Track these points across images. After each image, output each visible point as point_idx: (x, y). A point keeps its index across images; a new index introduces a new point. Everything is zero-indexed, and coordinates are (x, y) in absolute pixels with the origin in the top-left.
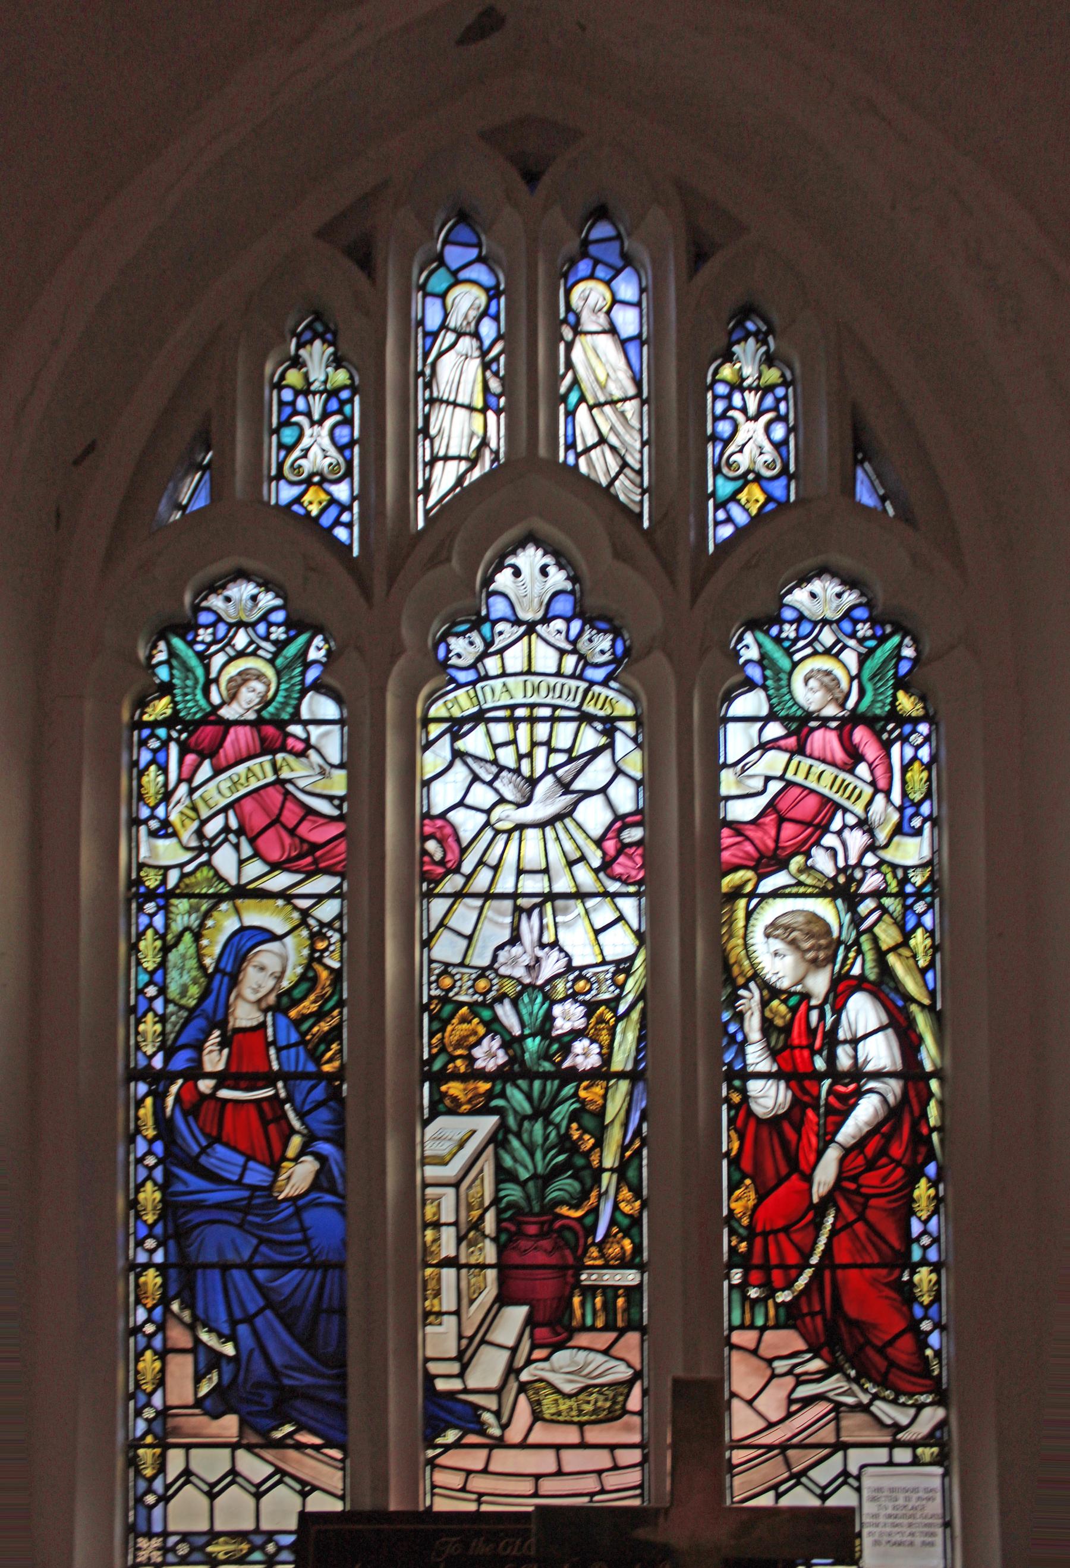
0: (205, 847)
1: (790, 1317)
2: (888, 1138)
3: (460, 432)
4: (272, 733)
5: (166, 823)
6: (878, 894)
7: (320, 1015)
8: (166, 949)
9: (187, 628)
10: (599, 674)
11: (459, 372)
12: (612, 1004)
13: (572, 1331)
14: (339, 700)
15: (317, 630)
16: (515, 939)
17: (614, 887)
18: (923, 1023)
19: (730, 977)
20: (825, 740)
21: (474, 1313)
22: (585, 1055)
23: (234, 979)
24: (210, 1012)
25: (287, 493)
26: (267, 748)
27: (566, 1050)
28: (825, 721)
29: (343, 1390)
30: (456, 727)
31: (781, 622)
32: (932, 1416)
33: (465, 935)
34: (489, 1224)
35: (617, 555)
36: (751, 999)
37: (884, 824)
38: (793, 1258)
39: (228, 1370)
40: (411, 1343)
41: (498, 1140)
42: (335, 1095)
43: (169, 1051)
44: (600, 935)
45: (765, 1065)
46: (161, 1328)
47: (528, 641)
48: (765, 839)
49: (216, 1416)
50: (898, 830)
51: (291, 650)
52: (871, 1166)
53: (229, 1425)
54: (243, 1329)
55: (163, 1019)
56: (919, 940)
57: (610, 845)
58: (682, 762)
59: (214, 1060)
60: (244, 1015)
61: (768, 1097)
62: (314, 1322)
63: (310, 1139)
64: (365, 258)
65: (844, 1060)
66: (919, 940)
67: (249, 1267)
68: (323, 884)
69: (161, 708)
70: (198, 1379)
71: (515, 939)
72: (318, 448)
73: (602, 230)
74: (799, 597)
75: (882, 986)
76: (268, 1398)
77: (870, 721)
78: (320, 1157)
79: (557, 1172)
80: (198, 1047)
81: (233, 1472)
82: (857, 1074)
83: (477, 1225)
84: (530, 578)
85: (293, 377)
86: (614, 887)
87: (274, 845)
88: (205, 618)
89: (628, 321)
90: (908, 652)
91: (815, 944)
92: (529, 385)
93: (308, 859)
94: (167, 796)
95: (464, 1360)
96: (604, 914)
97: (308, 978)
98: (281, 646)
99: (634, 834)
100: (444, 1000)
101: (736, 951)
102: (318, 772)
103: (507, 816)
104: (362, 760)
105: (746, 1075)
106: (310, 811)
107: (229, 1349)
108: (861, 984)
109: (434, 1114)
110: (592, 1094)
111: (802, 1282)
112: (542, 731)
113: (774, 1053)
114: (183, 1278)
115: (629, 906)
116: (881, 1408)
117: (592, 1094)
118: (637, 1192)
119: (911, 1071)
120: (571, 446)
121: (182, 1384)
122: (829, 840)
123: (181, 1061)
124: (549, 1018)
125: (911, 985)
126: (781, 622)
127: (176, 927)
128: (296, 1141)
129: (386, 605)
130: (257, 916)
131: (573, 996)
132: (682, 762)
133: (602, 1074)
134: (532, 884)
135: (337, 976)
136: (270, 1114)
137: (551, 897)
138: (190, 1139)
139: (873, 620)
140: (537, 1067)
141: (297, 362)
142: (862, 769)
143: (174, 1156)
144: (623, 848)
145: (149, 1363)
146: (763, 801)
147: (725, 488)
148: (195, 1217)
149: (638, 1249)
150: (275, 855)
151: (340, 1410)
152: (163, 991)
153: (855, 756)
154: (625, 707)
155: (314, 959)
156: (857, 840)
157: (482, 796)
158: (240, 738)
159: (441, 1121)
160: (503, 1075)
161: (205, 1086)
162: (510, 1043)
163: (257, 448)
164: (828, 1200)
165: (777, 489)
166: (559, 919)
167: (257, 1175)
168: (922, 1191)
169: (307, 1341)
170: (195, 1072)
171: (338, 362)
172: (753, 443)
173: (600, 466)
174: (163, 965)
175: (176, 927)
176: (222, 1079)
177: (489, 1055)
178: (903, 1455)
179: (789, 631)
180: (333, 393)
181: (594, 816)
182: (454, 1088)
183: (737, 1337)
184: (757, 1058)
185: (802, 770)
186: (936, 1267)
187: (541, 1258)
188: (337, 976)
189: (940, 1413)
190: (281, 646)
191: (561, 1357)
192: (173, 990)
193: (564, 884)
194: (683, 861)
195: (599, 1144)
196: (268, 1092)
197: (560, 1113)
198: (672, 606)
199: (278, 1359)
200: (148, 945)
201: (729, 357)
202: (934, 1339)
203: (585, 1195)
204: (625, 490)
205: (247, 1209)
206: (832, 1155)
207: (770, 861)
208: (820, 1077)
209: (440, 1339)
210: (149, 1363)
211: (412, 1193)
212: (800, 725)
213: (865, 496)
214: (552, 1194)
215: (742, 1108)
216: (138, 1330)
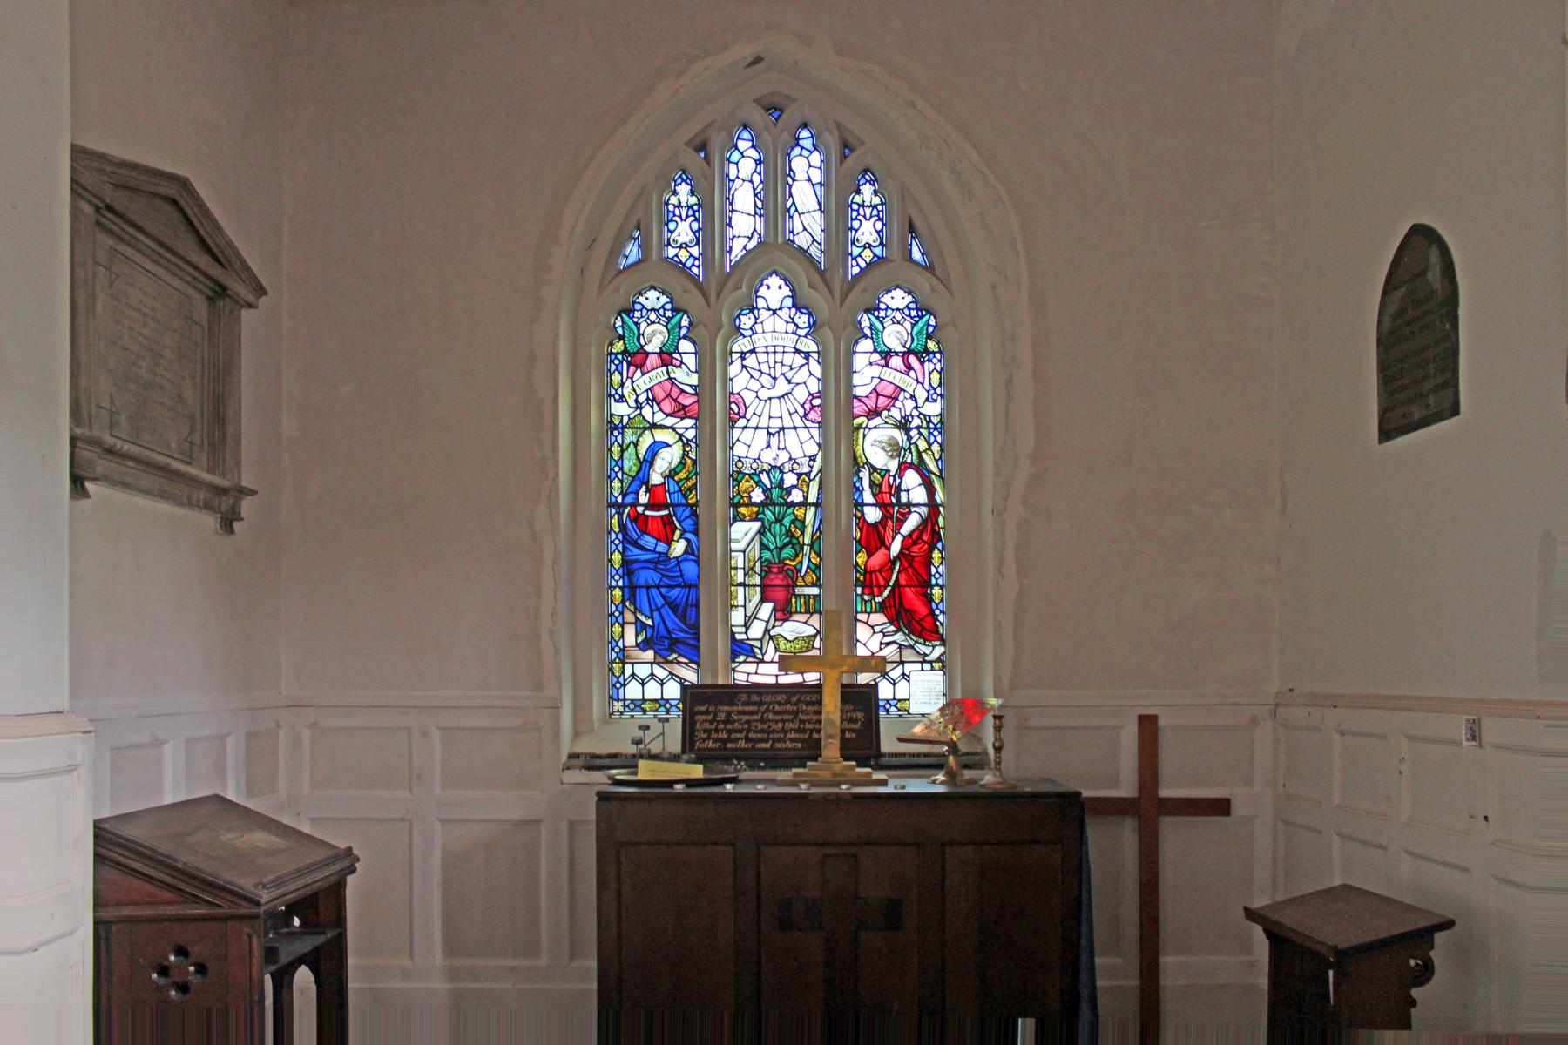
0: (639, 406)
1: (882, 608)
2: (921, 532)
3: (744, 226)
4: (667, 357)
5: (622, 396)
6: (918, 428)
7: (687, 479)
8: (623, 451)
9: (629, 311)
10: (803, 332)
11: (744, 198)
12: (808, 474)
13: (791, 614)
14: (694, 343)
15: (685, 312)
16: (768, 446)
17: (809, 424)
18: (937, 484)
19: (856, 463)
20: (896, 362)
21: (751, 607)
22: (796, 496)
23: (652, 464)
24: (641, 478)
25: (671, 252)
26: (665, 364)
27: (789, 494)
28: (896, 353)
29: (698, 640)
30: (743, 355)
31: (878, 309)
32: (939, 650)
33: (749, 446)
34: (757, 569)
35: (811, 286)
36: (865, 474)
37: (920, 393)
38: (882, 582)
39: (650, 631)
40: (727, 618)
41: (761, 532)
42: (694, 514)
43: (624, 495)
44: (803, 445)
45: (872, 501)
46: (622, 613)
47: (774, 323)
48: (871, 403)
49: (644, 650)
50: (927, 400)
51: (674, 321)
52: (915, 543)
53: (650, 655)
54: (656, 614)
55: (621, 481)
56: (936, 448)
57: (807, 406)
58: (838, 370)
59: (644, 498)
60: (656, 479)
61: (873, 515)
62: (685, 610)
63: (684, 532)
64: (702, 147)
65: (904, 499)
66: (936, 448)
67: (658, 587)
68: (689, 422)
69: (619, 347)
70: (637, 635)
71: (768, 446)
72: (683, 231)
73: (805, 134)
74: (886, 299)
75: (920, 468)
76: (666, 643)
77: (915, 354)
78: (688, 540)
79: (786, 545)
80: (637, 493)
81: (652, 674)
82: (909, 505)
83: (752, 569)
84: (774, 292)
85: (674, 200)
86: (809, 424)
87: (667, 406)
88: (638, 307)
89: (816, 176)
90: (933, 322)
91: (895, 450)
92: (774, 204)
93: (681, 411)
94: (622, 385)
95: (747, 626)
96: (804, 434)
97: (682, 463)
98: (669, 319)
99: (817, 402)
100: (739, 472)
101: (859, 451)
102: (686, 377)
103: (764, 394)
104: (705, 368)
105: (863, 505)
106: (683, 391)
107: (649, 622)
108: (911, 466)
109: (735, 520)
110: (800, 512)
111: (886, 593)
112: (779, 357)
113: (875, 496)
114: (631, 591)
115: (815, 432)
116: (918, 647)
117: (800, 512)
118: (818, 555)
119: (932, 505)
120: (791, 232)
121: (630, 637)
122: (898, 404)
123: (629, 499)
124: (782, 479)
125: (933, 467)
126: (878, 309)
127: (627, 441)
128: (678, 533)
129: (712, 301)
130: (661, 435)
131: (792, 471)
132: (838, 370)
133: (804, 504)
134: (776, 423)
135: (695, 462)
136: (667, 521)
137: (783, 429)
138: (633, 531)
139: (917, 309)
140: (777, 498)
141: (675, 193)
142: (912, 373)
143: (627, 540)
144: (813, 407)
145: (617, 629)
146: (871, 388)
147: (856, 251)
148: (637, 566)
149: (818, 579)
150: (668, 410)
151: (697, 648)
152: (621, 469)
153: (909, 367)
154: (813, 347)
155: (685, 455)
156: (910, 404)
157: (754, 385)
158: (653, 360)
159: (738, 524)
160: (763, 504)
161: (640, 509)
162: (766, 491)
163: (661, 233)
164: (898, 557)
165: (878, 251)
166: (775, 401)
167: (661, 547)
168: (936, 555)
169: (683, 618)
170: (635, 504)
171: (692, 193)
172: (867, 231)
173: (802, 240)
174: (621, 457)
175: (627, 441)
176: (647, 507)
177: (757, 496)
178: (927, 666)
179: (882, 314)
180: (690, 207)
181: (801, 394)
182: (743, 510)
183: (860, 617)
184: (868, 497)
185: (887, 374)
186: (942, 587)
187: (778, 582)
188: (695, 462)
189: (942, 649)
190: (669, 319)
191: (787, 624)
192: (626, 469)
193: (788, 423)
194: (837, 412)
195: (803, 533)
196: (665, 512)
197: (787, 521)
198: (834, 300)
199: (670, 626)
200: (616, 449)
201: (858, 192)
202: (940, 618)
203: (797, 555)
204: (815, 251)
205: (658, 562)
206: (899, 539)
207: (873, 413)
208: (893, 505)
209: (737, 617)
210: (617, 629)
211: (728, 553)
212: (886, 355)
213: (916, 255)
214: (784, 554)
215: (862, 520)
216: (612, 614)
